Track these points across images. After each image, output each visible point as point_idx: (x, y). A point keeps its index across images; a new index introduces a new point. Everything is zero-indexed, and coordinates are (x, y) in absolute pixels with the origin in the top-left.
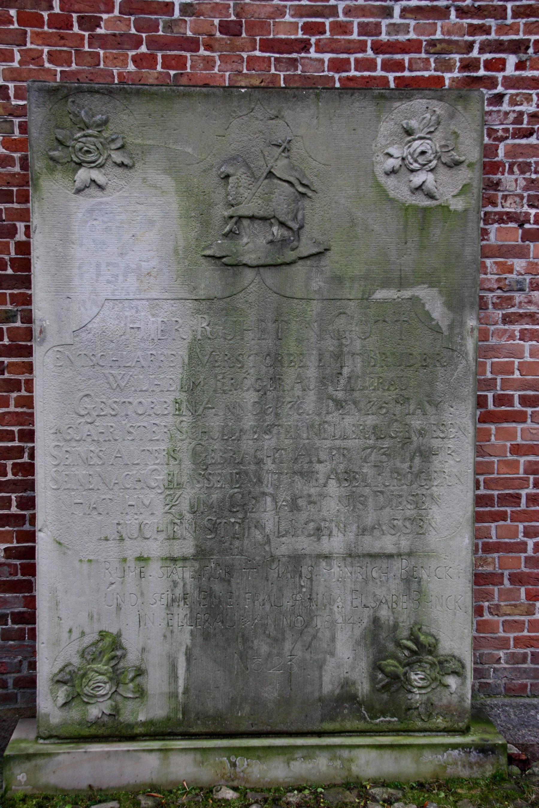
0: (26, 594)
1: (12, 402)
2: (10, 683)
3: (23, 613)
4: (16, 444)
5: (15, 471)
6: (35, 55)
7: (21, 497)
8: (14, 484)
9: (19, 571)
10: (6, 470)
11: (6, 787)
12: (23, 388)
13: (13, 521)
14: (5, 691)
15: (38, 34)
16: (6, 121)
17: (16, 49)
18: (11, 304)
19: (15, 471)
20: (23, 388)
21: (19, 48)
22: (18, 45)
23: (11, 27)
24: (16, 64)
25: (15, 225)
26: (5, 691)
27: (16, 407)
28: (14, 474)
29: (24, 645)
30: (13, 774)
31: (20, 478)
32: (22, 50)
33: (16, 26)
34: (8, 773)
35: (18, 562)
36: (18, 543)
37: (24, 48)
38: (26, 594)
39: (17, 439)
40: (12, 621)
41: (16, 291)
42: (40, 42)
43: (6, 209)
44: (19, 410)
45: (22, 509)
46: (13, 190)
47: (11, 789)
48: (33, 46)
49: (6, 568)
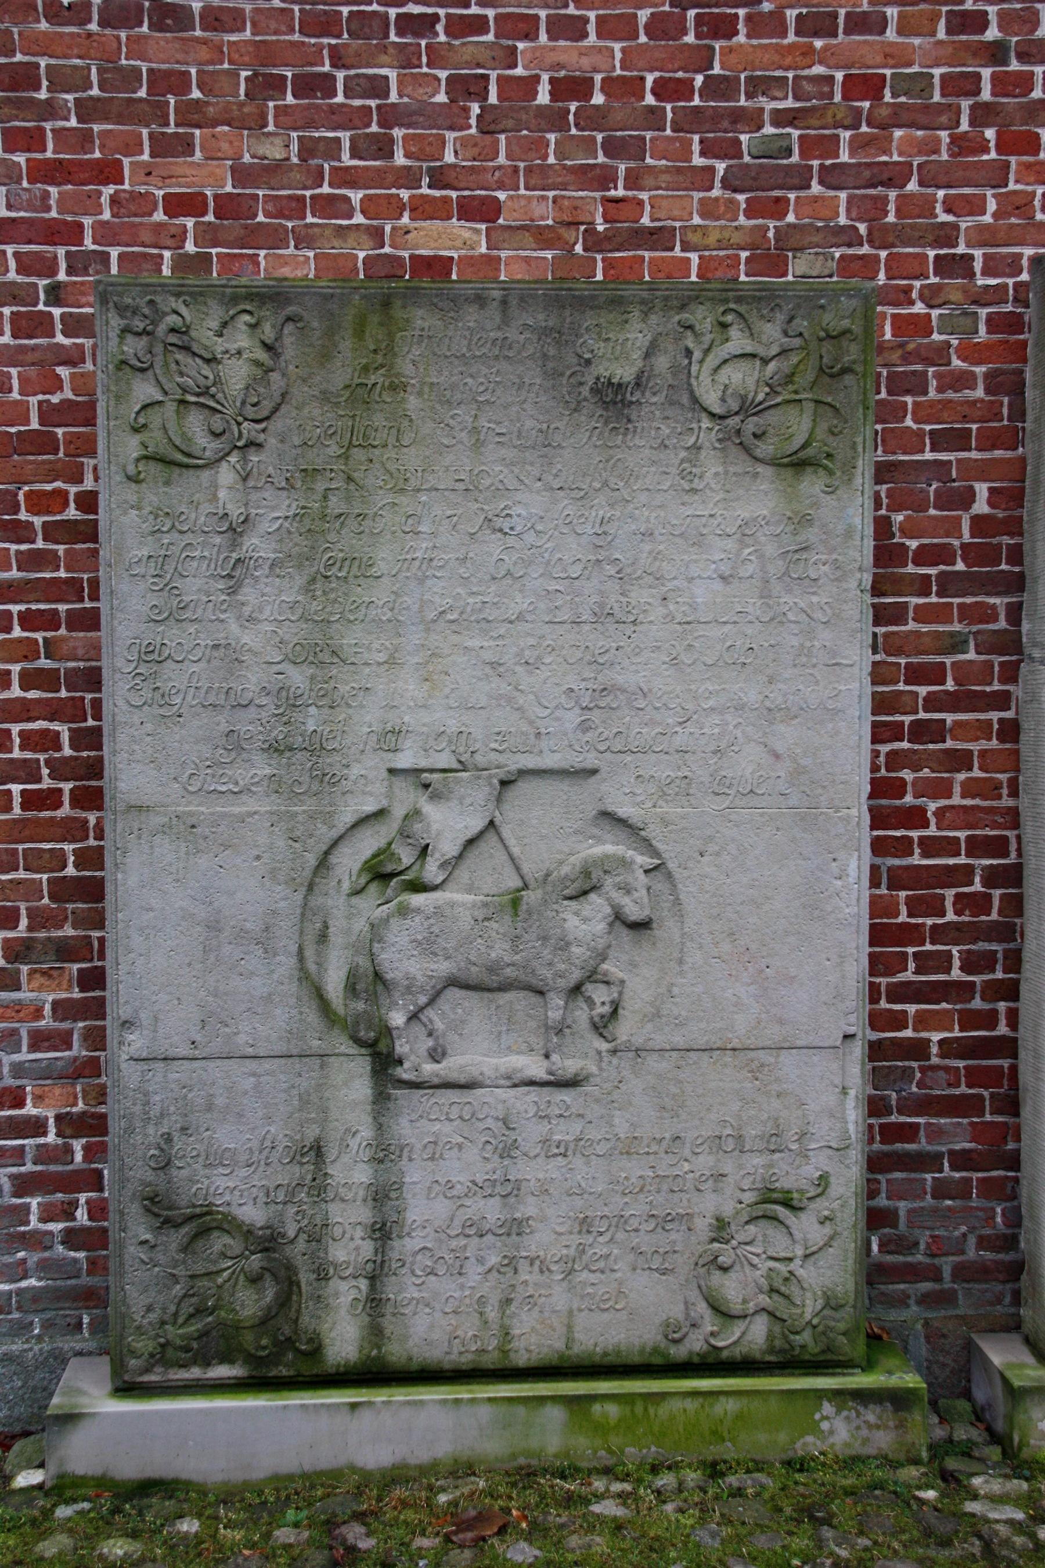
0: (975, 1120)
1: (957, 789)
2: (947, 1273)
3: (970, 1151)
4: (962, 860)
5: (958, 906)
6: (1020, 201)
7: (969, 951)
8: (958, 930)
9: (963, 1079)
10: (944, 906)
11: (1021, 1441)
12: (976, 765)
13: (954, 994)
14: (937, 1287)
15: (1028, 166)
16: (965, 314)
17: (989, 193)
18: (960, 622)
19: (958, 906)
20: (976, 765)
21: (993, 191)
22: (993, 187)
23: (985, 157)
24: (988, 219)
25: (972, 488)
26: (937, 1287)
27: (963, 797)
28: (957, 913)
29: (971, 1208)
30: (1030, 1419)
31: (967, 919)
32: (1000, 194)
33: (993, 155)
34: (1022, 1416)
35: (961, 1064)
36: (961, 1030)
37: (1003, 190)
38: (975, 1120)
39: (963, 852)
40: (951, 1166)
41: (969, 600)
42: (1032, 179)
43: (958, 461)
44: (968, 802)
45: (969, 973)
46: (970, 429)
47: (1028, 1445)
48: (1019, 187)
49: (941, 1074)
